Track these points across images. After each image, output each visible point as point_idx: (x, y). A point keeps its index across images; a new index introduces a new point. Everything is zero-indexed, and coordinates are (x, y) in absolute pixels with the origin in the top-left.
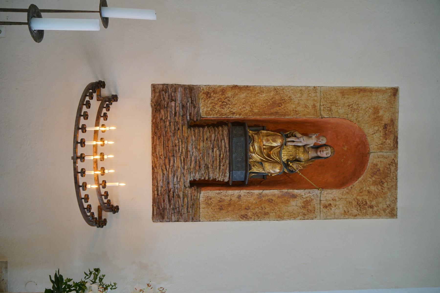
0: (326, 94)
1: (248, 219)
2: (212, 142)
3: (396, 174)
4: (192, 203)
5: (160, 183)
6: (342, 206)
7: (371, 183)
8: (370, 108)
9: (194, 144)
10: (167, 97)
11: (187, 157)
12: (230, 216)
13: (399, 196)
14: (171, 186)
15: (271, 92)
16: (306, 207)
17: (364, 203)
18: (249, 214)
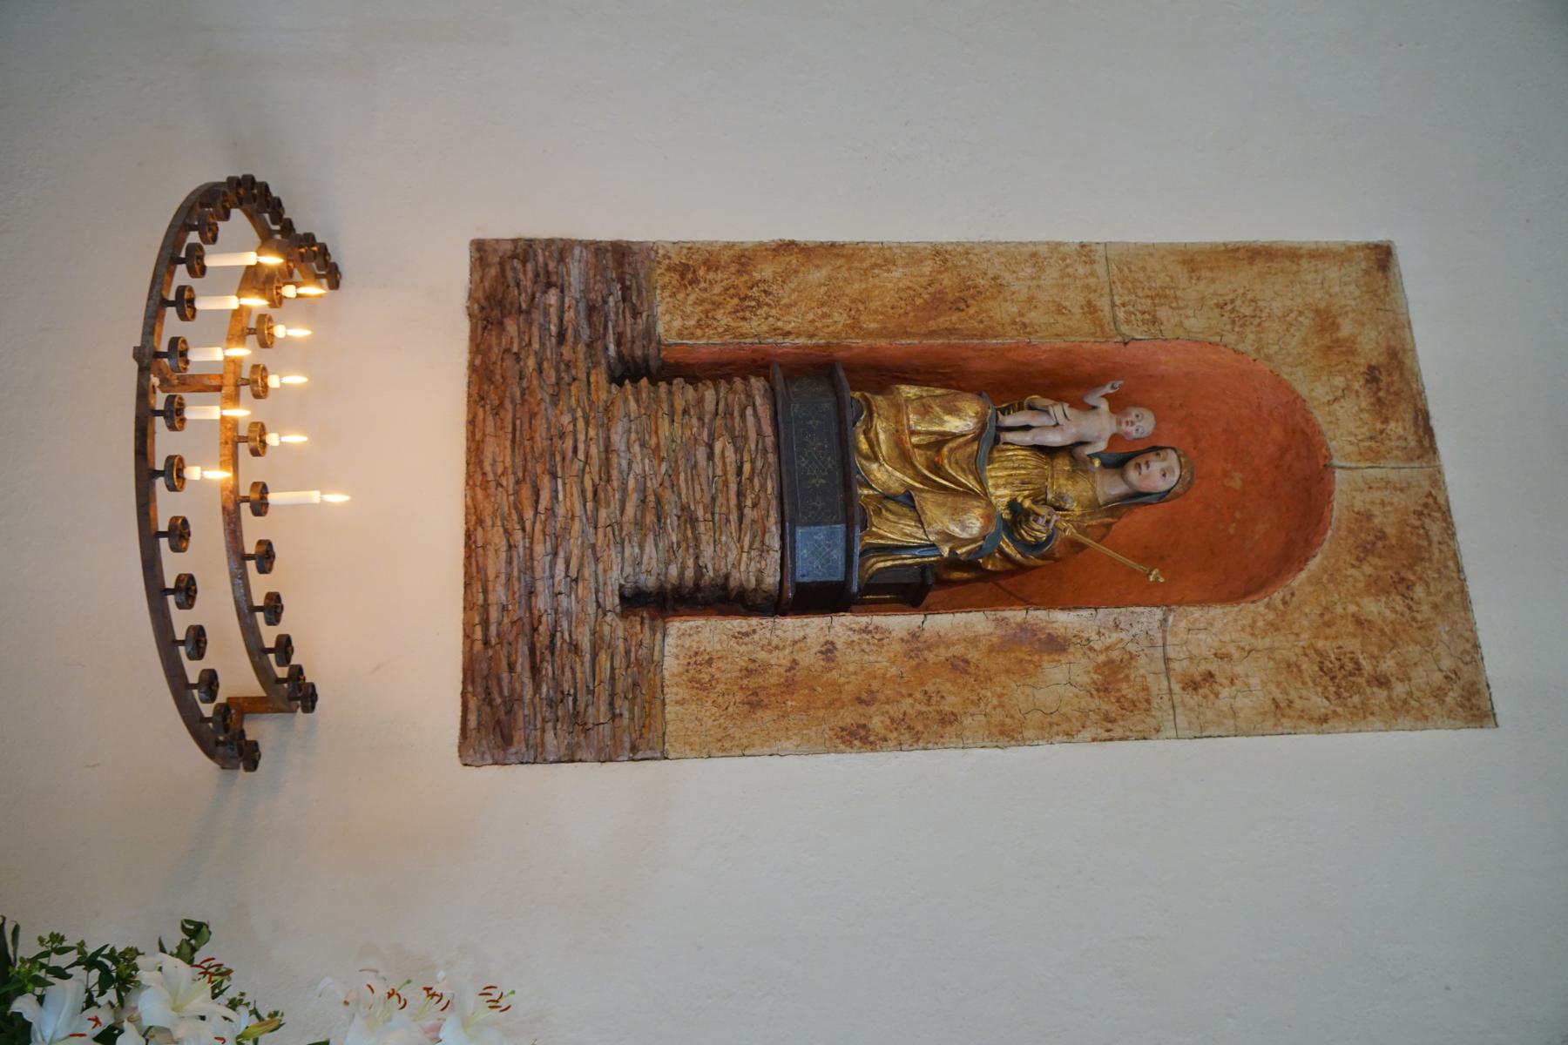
0: (1129, 268)
1: (871, 743)
2: (706, 420)
3: (1455, 551)
4: (630, 680)
5: (494, 587)
6: (1262, 681)
7: (1361, 585)
8: (1301, 313)
9: (633, 430)
10: (530, 275)
11: (609, 480)
12: (795, 734)
13: (1483, 637)
14: (542, 602)
15: (922, 262)
16: (1111, 687)
17: (1350, 666)
18: (877, 723)
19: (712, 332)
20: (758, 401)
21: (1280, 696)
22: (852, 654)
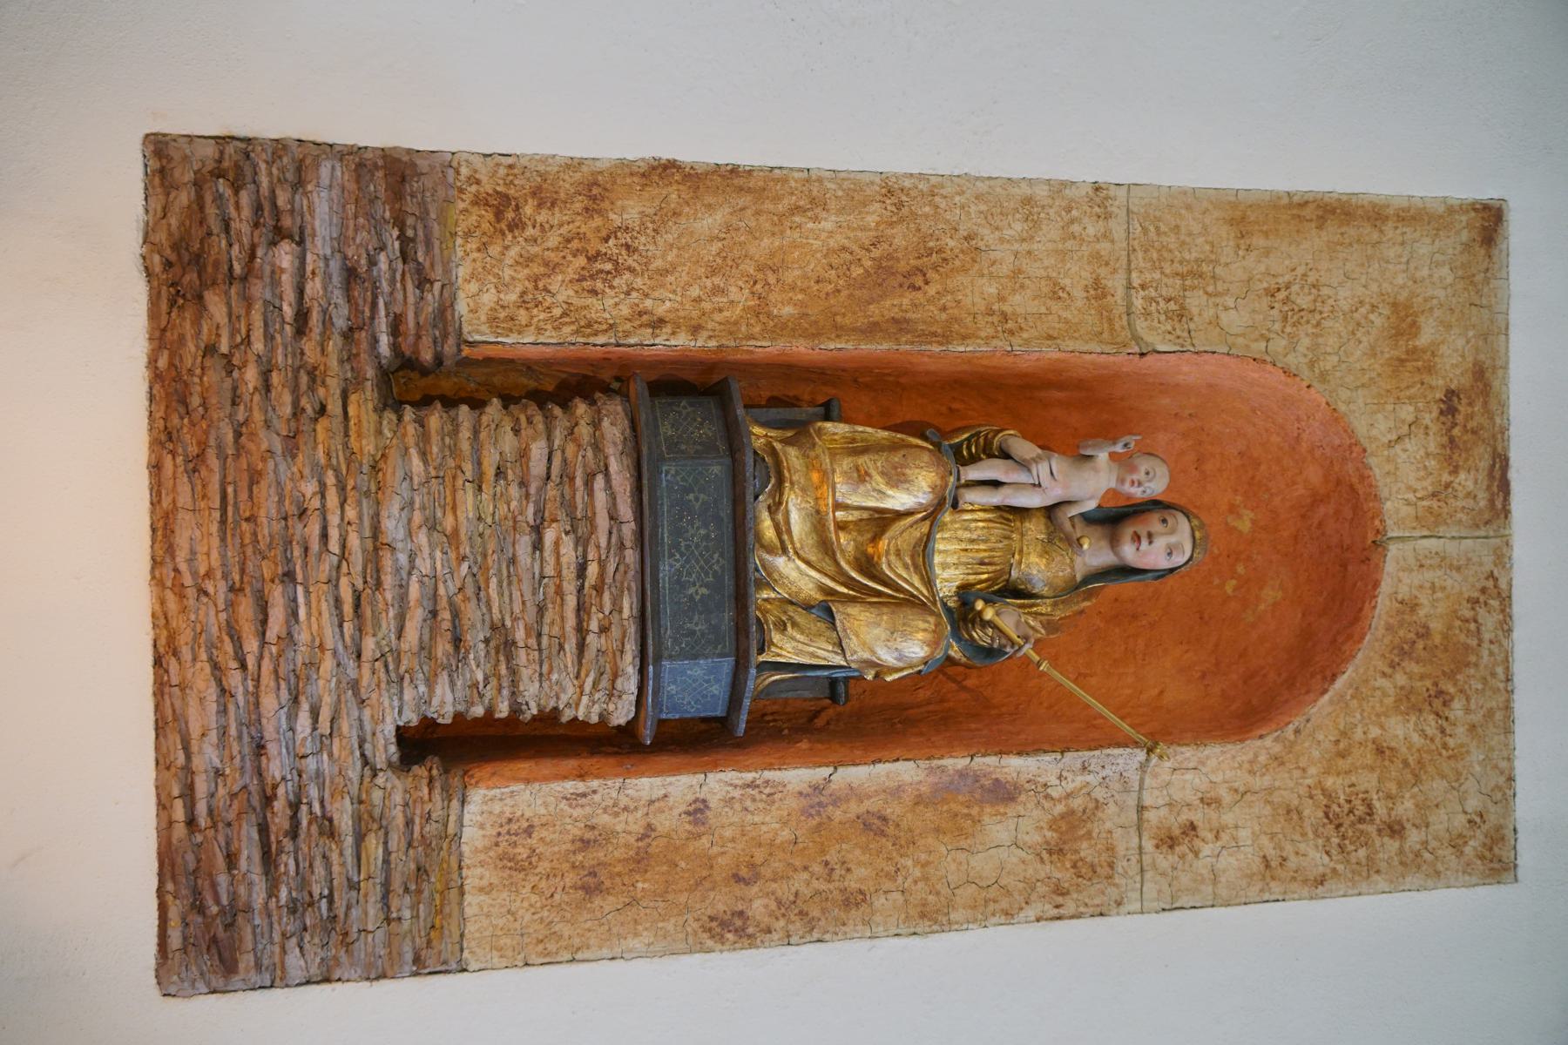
0: (1157, 228)
1: (749, 936)
2: (532, 490)
5: (200, 748)
6: (1253, 833)
7: (1389, 701)
8: (1374, 307)
10: (246, 212)
11: (379, 584)
14: (276, 767)
17: (1361, 810)
18: (758, 908)
19: (542, 316)
20: (614, 466)
21: (1273, 852)
22: (730, 814)
